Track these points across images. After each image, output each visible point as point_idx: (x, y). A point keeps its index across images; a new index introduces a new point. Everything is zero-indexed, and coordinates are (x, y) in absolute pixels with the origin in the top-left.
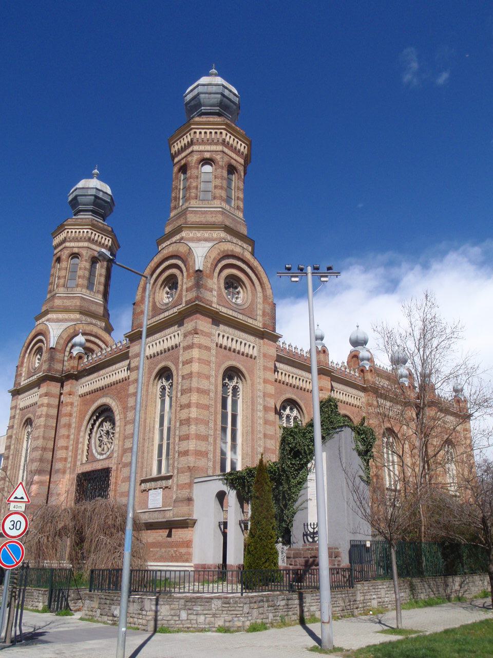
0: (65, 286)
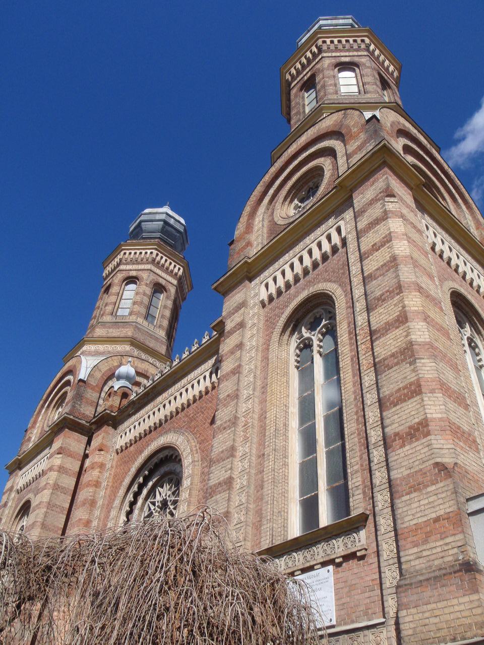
0: (114, 314)
